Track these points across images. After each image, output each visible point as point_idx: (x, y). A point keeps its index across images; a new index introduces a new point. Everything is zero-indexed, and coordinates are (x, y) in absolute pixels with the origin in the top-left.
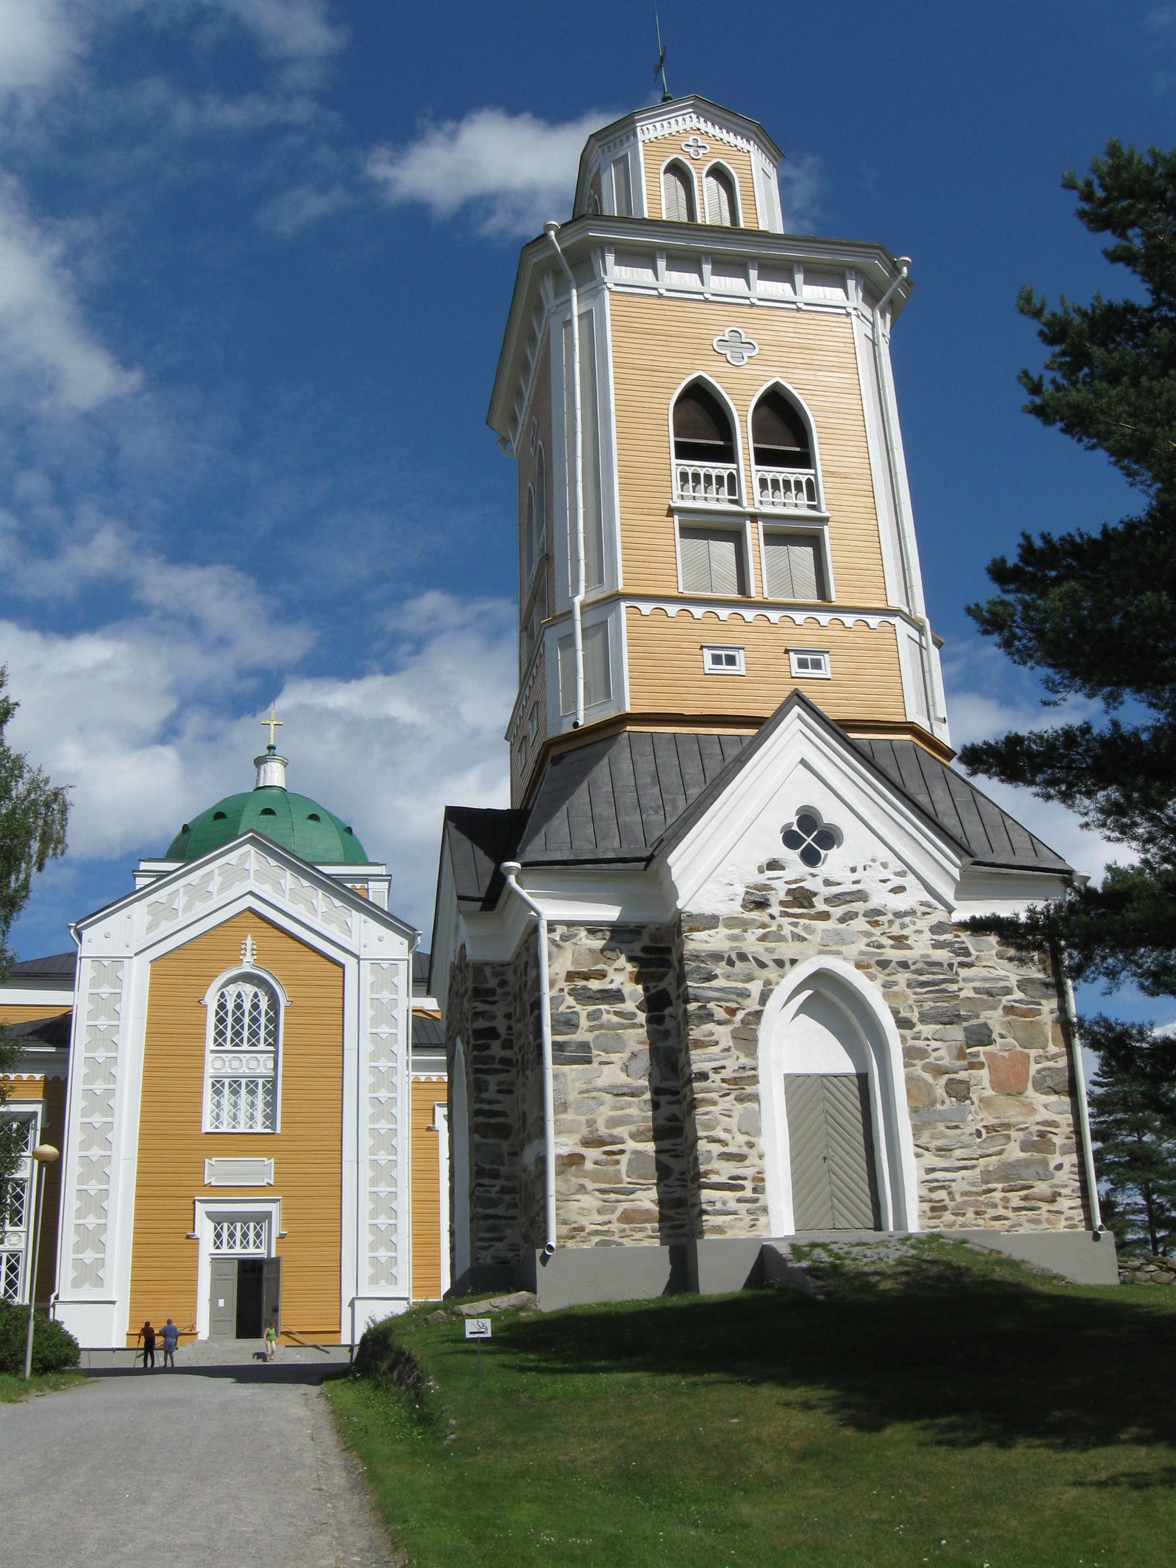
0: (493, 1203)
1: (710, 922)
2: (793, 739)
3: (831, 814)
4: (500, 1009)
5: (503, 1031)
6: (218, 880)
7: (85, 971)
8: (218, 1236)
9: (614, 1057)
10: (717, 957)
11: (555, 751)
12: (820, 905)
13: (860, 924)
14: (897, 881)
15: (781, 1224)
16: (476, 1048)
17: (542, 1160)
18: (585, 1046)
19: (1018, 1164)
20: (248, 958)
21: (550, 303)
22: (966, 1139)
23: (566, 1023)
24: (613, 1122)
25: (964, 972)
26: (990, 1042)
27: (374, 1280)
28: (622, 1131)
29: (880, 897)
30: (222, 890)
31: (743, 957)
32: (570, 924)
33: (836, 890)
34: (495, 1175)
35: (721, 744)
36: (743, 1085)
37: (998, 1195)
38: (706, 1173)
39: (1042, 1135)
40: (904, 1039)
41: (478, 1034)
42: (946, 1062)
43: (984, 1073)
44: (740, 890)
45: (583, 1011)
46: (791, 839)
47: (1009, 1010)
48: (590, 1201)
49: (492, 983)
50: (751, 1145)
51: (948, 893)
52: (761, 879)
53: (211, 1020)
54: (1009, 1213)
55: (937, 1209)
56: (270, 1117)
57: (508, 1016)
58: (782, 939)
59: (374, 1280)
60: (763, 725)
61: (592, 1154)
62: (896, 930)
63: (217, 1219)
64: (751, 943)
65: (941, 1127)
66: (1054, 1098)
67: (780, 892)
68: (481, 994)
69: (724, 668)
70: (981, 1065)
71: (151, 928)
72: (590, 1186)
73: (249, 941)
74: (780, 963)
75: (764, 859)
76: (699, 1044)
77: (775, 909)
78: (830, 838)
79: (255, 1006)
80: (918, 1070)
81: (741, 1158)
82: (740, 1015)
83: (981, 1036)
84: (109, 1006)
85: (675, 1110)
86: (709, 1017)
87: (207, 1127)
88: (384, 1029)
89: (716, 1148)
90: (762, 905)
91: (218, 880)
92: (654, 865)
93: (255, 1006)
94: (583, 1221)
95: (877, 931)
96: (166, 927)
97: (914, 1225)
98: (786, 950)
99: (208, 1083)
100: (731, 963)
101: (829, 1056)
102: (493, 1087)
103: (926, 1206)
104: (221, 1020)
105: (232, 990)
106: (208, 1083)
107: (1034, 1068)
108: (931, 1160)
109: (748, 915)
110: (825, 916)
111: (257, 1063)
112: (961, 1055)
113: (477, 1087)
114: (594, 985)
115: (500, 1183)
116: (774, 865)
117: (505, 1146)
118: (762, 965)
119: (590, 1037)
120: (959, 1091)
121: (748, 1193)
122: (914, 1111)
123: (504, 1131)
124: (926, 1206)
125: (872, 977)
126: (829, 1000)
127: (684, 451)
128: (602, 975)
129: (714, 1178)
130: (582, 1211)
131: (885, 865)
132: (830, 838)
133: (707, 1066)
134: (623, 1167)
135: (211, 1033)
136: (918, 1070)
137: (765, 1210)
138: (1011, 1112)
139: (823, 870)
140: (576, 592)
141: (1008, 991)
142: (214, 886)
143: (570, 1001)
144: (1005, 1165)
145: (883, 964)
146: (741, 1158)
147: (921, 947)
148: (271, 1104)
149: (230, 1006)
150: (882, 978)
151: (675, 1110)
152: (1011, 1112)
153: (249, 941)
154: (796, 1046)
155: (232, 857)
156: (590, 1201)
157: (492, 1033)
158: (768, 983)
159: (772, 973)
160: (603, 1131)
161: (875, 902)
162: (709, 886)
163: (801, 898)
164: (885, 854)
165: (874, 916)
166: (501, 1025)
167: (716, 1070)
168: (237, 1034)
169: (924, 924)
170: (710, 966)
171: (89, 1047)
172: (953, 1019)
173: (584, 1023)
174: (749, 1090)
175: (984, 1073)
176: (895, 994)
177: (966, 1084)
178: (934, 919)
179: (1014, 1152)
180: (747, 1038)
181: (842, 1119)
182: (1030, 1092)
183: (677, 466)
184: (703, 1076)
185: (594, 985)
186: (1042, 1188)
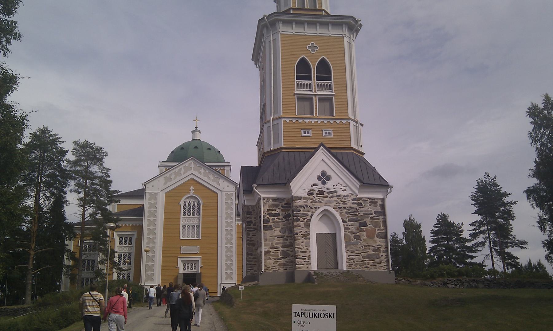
0: (251, 261)
1: (300, 198)
2: (321, 155)
3: (329, 172)
4: (253, 216)
5: (254, 222)
6: (183, 171)
7: (147, 196)
8: (185, 267)
9: (277, 229)
10: (301, 206)
11: (266, 155)
12: (326, 194)
13: (335, 198)
14: (345, 188)
15: (314, 266)
16: (248, 225)
17: (261, 252)
18: (271, 226)
19: (372, 255)
20: (192, 192)
21: (265, 36)
22: (358, 249)
23: (267, 221)
24: (277, 244)
25: (361, 209)
26: (367, 226)
27: (226, 279)
28: (279, 246)
29: (340, 192)
30: (184, 173)
31: (307, 206)
32: (268, 198)
33: (329, 190)
34: (251, 255)
35: (305, 155)
36: (306, 236)
37: (366, 262)
38: (297, 256)
39: (378, 248)
40: (344, 225)
41: (248, 222)
42: (354, 231)
43: (365, 233)
44: (307, 191)
45: (271, 218)
46: (319, 178)
47: (371, 218)
48: (271, 261)
49: (251, 210)
50: (308, 249)
51: (357, 192)
52: (312, 188)
53: (182, 209)
54: (369, 266)
55: (351, 265)
56: (198, 235)
57: (255, 218)
58: (316, 202)
59: (226, 279)
60: (316, 149)
61: (272, 251)
62: (343, 200)
63: (184, 262)
64: (309, 203)
65: (352, 246)
66: (382, 239)
67: (316, 190)
68: (249, 213)
69: (307, 135)
70: (364, 231)
71: (165, 184)
72: (272, 258)
73: (192, 187)
74: (316, 208)
75: (313, 184)
76: (296, 226)
77: (315, 195)
78: (329, 178)
79: (194, 205)
80: (347, 233)
81: (305, 252)
82: (306, 220)
83: (365, 224)
84: (154, 205)
85: (292, 241)
86: (299, 220)
87: (181, 238)
88: (229, 211)
89: (300, 250)
90: (312, 194)
91: (183, 171)
92: (287, 184)
93: (194, 205)
94: (270, 266)
95: (339, 200)
96: (169, 184)
97: (344, 267)
98: (317, 205)
99: (181, 226)
100: (304, 208)
101: (325, 230)
102: (251, 235)
103: (348, 264)
104: (185, 209)
105: (188, 200)
106: (181, 226)
107: (377, 232)
108: (350, 253)
109: (308, 197)
110: (327, 197)
111: (194, 220)
112: (358, 229)
113: (248, 234)
114: (273, 212)
115: (252, 256)
116: (315, 185)
117: (254, 248)
118: (311, 208)
119: (272, 224)
120: (357, 238)
121: (307, 260)
122: (346, 242)
123: (253, 245)
124: (348, 264)
125: (337, 211)
126: (326, 215)
127: (298, 78)
128: (275, 210)
129: (299, 257)
130: (270, 264)
131: (341, 185)
132: (329, 178)
133: (298, 231)
134: (279, 254)
135: (182, 212)
136: (347, 233)
137: (310, 264)
138: (371, 242)
139: (327, 186)
140: (271, 116)
141: (371, 214)
142: (182, 172)
143: (268, 216)
144: (369, 255)
145: (340, 208)
146: (305, 252)
147: (349, 204)
148: (198, 231)
149: (187, 205)
150: (340, 211)
151: (292, 241)
152: (371, 242)
153: (192, 187)
154: (317, 227)
155: (187, 164)
156: (271, 261)
157: (251, 222)
158: (312, 212)
159: (314, 210)
160: (275, 245)
161: (339, 193)
162: (300, 190)
163: (321, 192)
164: (341, 182)
165: (338, 196)
166: (253, 220)
167: (300, 232)
168: (189, 212)
169: (350, 199)
170: (299, 208)
171: (149, 217)
172: (356, 221)
173: (271, 221)
174: (307, 237)
175: (365, 233)
176: (343, 215)
177: (359, 236)
178: (353, 197)
179: (371, 252)
180: (307, 225)
181: (328, 243)
182: (376, 238)
183: (296, 81)
184: (297, 234)
185: (273, 212)
186: (377, 260)
